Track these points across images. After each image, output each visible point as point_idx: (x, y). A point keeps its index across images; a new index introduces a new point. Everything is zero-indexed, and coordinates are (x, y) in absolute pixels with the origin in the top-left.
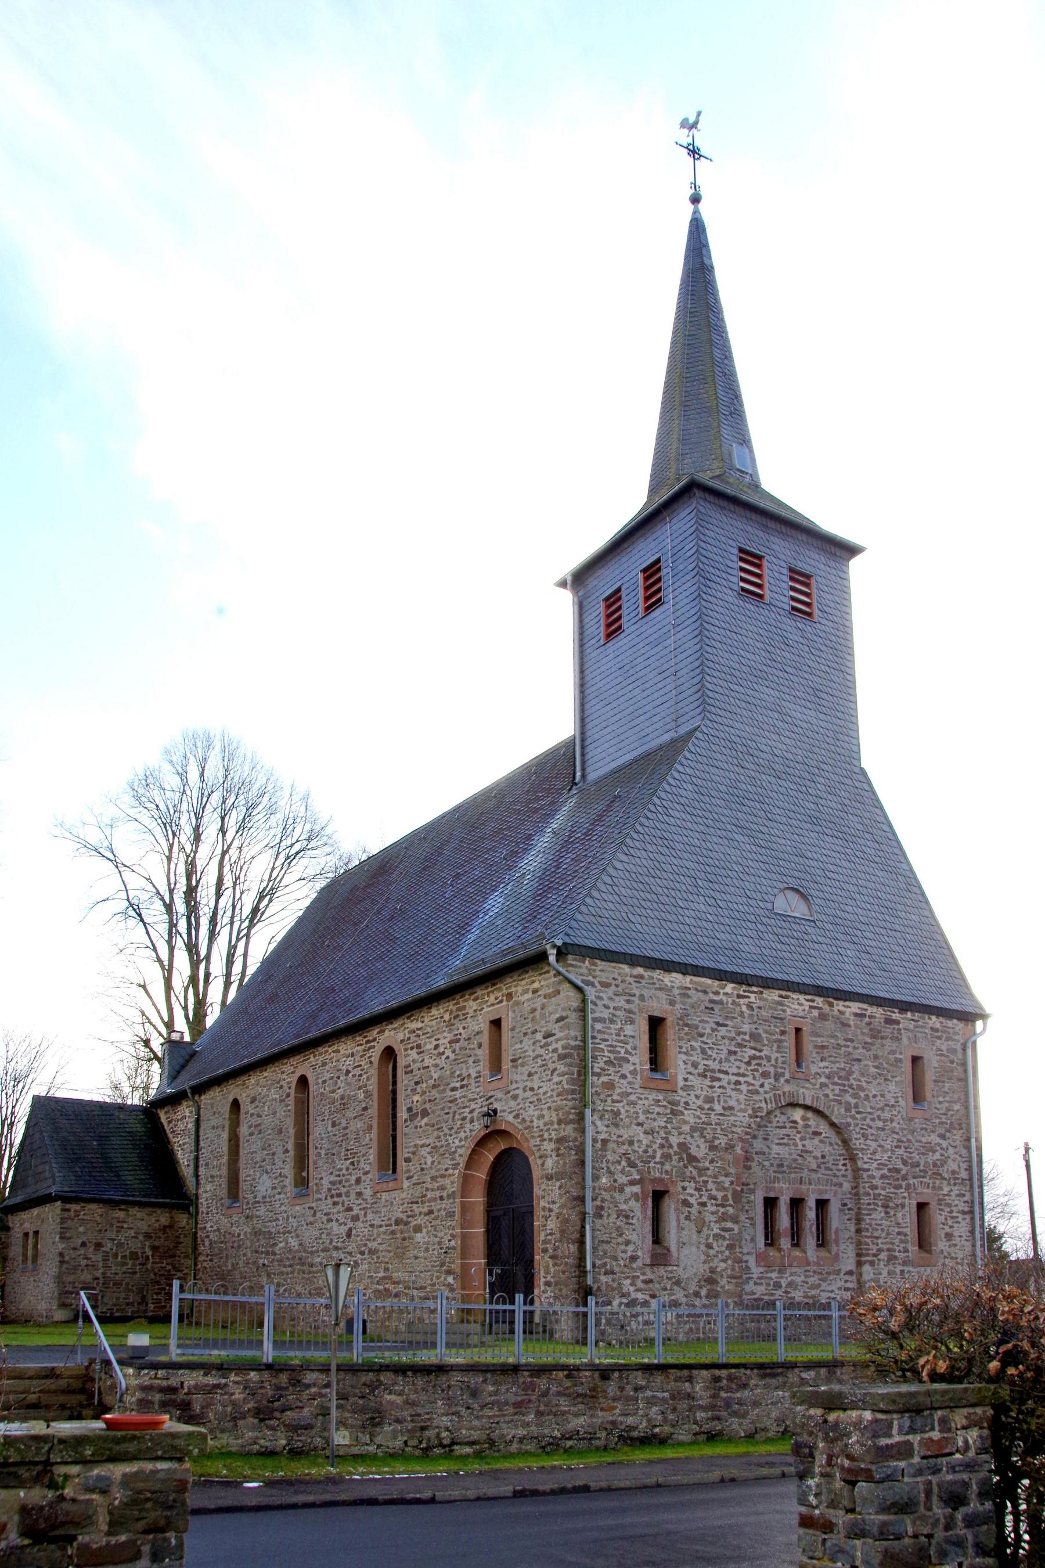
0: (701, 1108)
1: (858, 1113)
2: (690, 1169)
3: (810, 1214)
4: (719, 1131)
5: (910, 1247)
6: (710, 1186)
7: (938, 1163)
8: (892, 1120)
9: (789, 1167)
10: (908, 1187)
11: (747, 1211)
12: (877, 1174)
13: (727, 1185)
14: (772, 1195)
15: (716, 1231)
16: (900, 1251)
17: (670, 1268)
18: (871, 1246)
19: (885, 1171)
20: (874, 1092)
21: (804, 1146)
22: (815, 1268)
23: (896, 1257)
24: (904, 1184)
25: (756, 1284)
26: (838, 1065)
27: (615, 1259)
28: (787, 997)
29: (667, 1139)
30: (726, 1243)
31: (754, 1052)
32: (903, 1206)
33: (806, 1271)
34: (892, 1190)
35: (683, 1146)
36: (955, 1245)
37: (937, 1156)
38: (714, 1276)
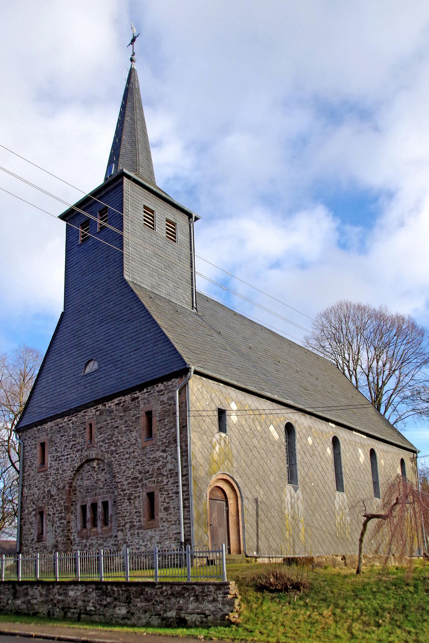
0: (55, 474)
1: (117, 454)
2: (51, 500)
3: (100, 510)
4: (60, 482)
5: (142, 519)
6: (57, 506)
7: (161, 467)
8: (134, 452)
9: (91, 489)
10: (143, 485)
11: (74, 513)
12: (125, 483)
13: (62, 504)
14: (84, 504)
15: (58, 524)
16: (137, 522)
17: (43, 542)
18: (122, 521)
19: (130, 480)
20: (125, 440)
21: (97, 477)
22: (101, 536)
23: (134, 526)
24: (140, 485)
25: (78, 546)
26: (107, 434)
27: (28, 541)
28: (87, 412)
29: (44, 490)
30: (61, 529)
31: (73, 442)
32: (139, 497)
33: (97, 538)
34: (134, 489)
35: (49, 491)
36: (170, 514)
37: (160, 463)
38: (57, 544)
